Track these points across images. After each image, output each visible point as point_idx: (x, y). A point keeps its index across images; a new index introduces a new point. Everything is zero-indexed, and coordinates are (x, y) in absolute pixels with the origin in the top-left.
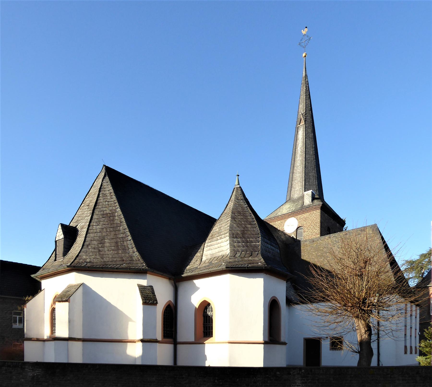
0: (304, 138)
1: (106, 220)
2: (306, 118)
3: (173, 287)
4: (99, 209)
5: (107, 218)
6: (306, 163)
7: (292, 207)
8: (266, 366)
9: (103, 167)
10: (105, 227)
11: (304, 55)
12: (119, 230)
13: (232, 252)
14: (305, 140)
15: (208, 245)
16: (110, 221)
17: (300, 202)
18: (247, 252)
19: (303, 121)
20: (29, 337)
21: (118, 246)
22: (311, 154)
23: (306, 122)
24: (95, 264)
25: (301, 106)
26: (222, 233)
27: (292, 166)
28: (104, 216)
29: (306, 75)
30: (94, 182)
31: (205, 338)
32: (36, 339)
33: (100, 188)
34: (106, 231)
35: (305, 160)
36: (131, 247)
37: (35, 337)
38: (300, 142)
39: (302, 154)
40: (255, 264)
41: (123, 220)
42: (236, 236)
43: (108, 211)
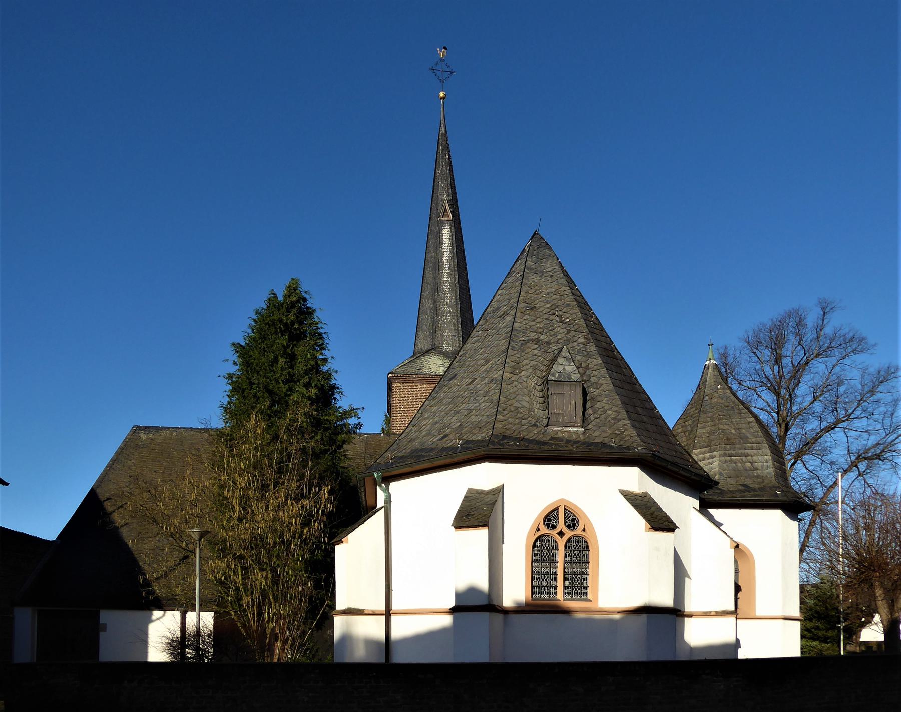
11: (442, 94)
29: (446, 131)
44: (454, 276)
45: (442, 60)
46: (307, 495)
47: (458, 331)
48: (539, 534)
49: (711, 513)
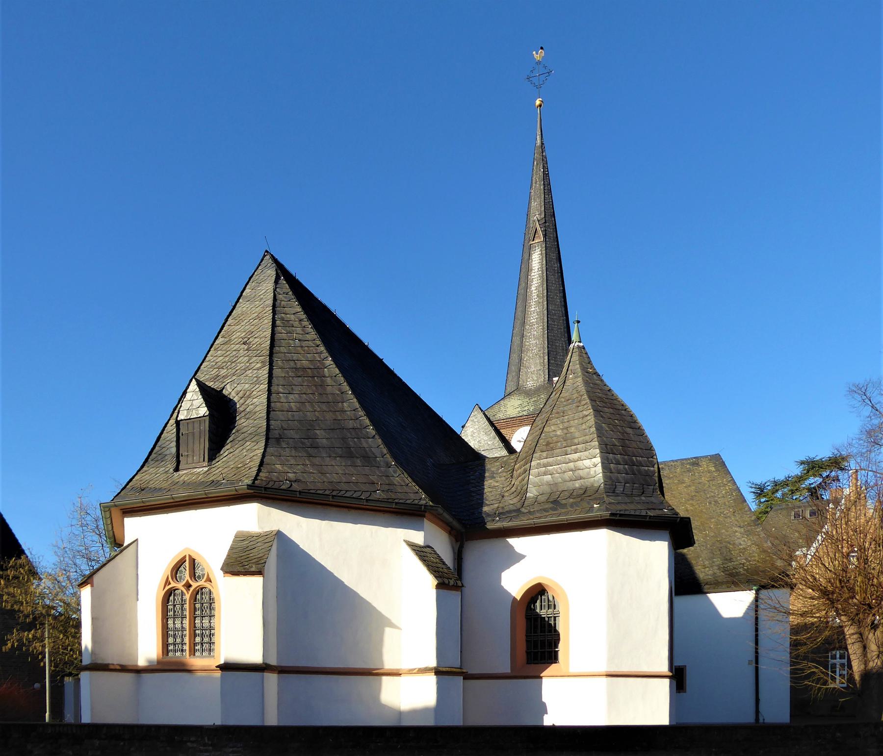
0: (544, 269)
1: (305, 384)
2: (546, 230)
3: (454, 553)
4: (283, 355)
5: (306, 378)
6: (549, 319)
7: (526, 404)
8: (282, 724)
9: (265, 256)
10: (307, 400)
11: (538, 102)
12: (343, 411)
13: (607, 483)
14: (546, 273)
15: (542, 464)
16: (315, 386)
17: (543, 396)
18: (635, 485)
19: (540, 233)
20: (100, 662)
21: (350, 448)
22: (557, 304)
23: (546, 239)
24: (311, 486)
25: (536, 203)
26: (576, 441)
27: (519, 322)
28: (299, 374)
29: (542, 144)
30: (244, 289)
31: (529, 666)
32: (118, 667)
33: (274, 306)
34: (311, 410)
35: (548, 314)
36: (381, 454)
37: (115, 663)
38: (536, 277)
39: (541, 301)
40: (657, 510)
41: (346, 387)
42: (612, 449)
43: (305, 363)
44: (543, 303)
45: (539, 63)
46: (254, 561)
47: (544, 364)
48: (167, 588)
49: (510, 543)
